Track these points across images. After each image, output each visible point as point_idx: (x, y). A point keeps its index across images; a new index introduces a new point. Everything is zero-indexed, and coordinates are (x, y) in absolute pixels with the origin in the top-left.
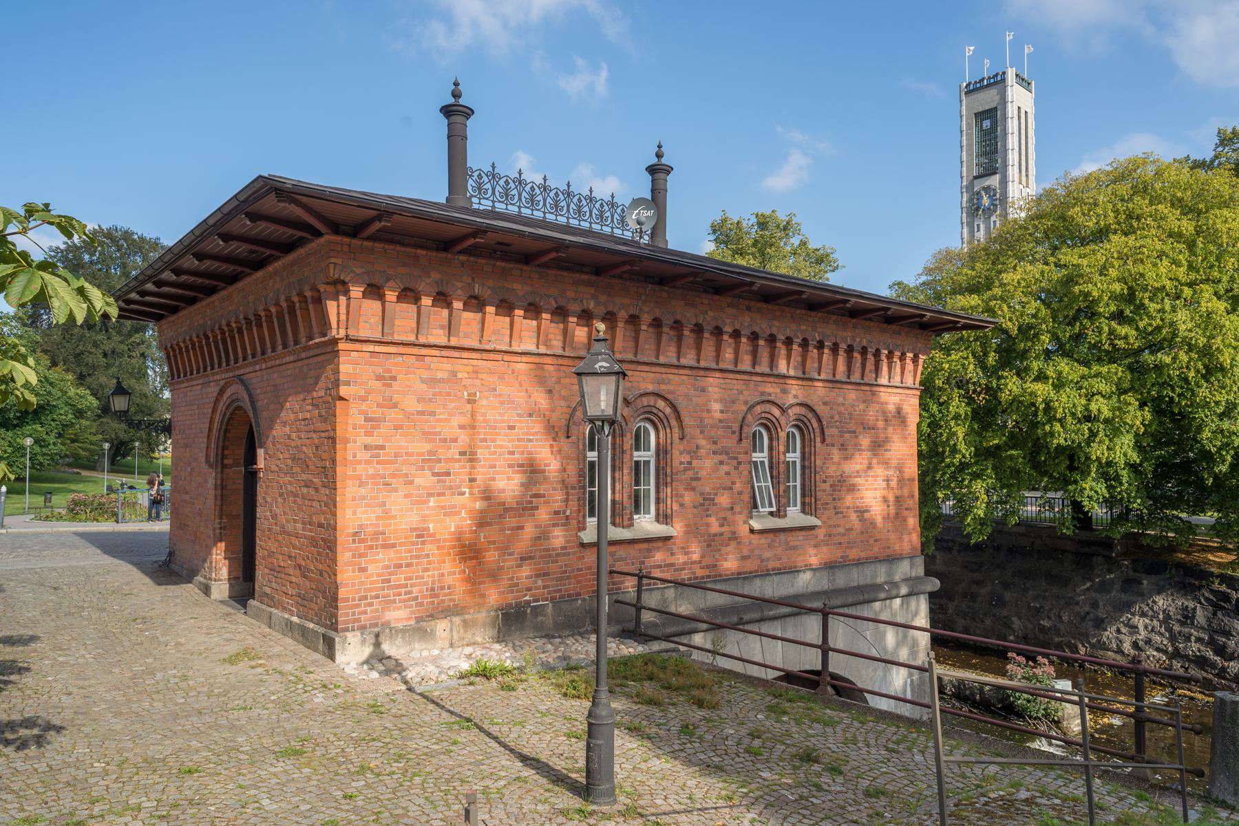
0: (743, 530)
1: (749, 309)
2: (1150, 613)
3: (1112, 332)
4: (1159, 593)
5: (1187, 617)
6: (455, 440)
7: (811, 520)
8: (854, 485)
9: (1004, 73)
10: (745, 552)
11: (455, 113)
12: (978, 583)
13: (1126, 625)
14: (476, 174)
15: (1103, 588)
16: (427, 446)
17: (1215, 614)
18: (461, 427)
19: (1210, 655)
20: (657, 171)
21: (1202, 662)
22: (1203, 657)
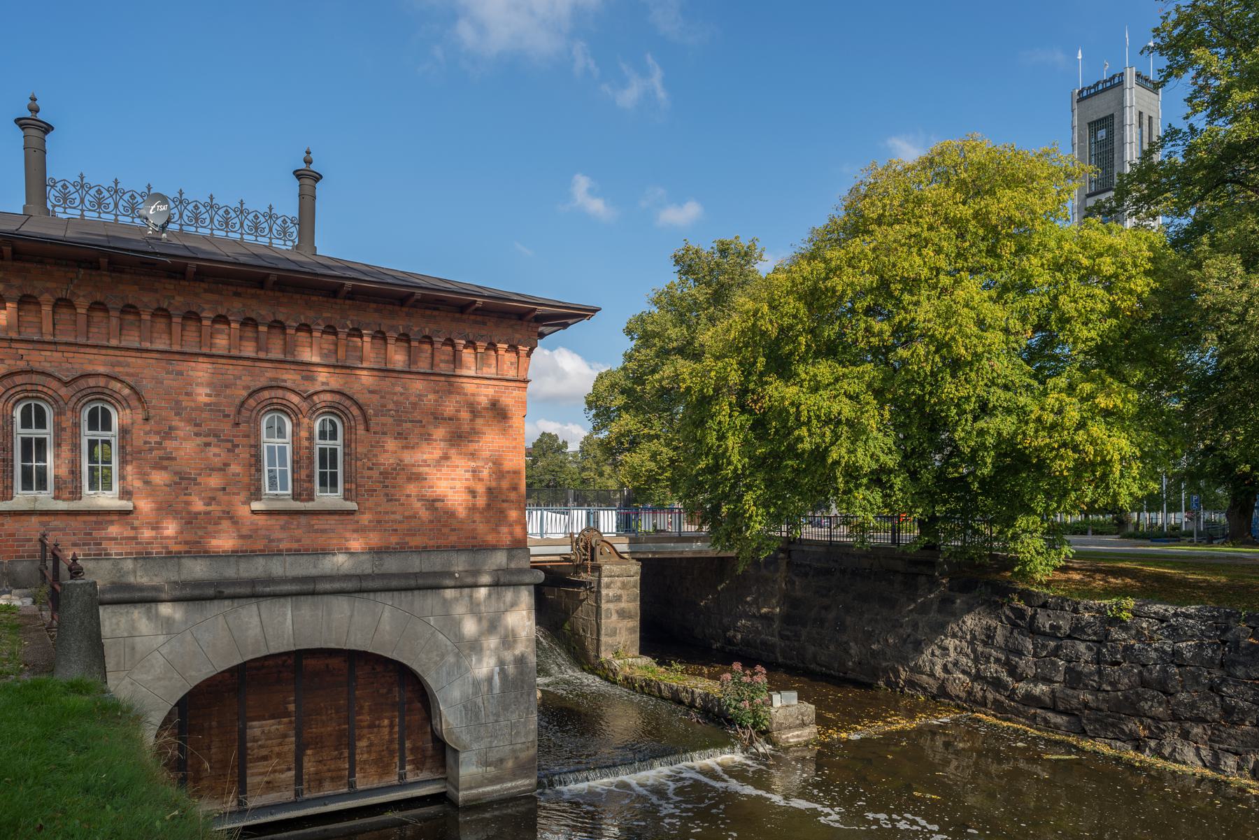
0: (243, 511)
1: (237, 294)
2: (960, 634)
3: (867, 330)
4: (968, 612)
5: (989, 635)
7: (352, 506)
8: (420, 474)
9: (1122, 74)
10: (245, 532)
11: (35, 128)
12: (826, 608)
13: (940, 647)
14: (59, 185)
15: (923, 609)
17: (1011, 633)
19: (1004, 676)
20: (307, 177)
21: (997, 684)
22: (998, 678)
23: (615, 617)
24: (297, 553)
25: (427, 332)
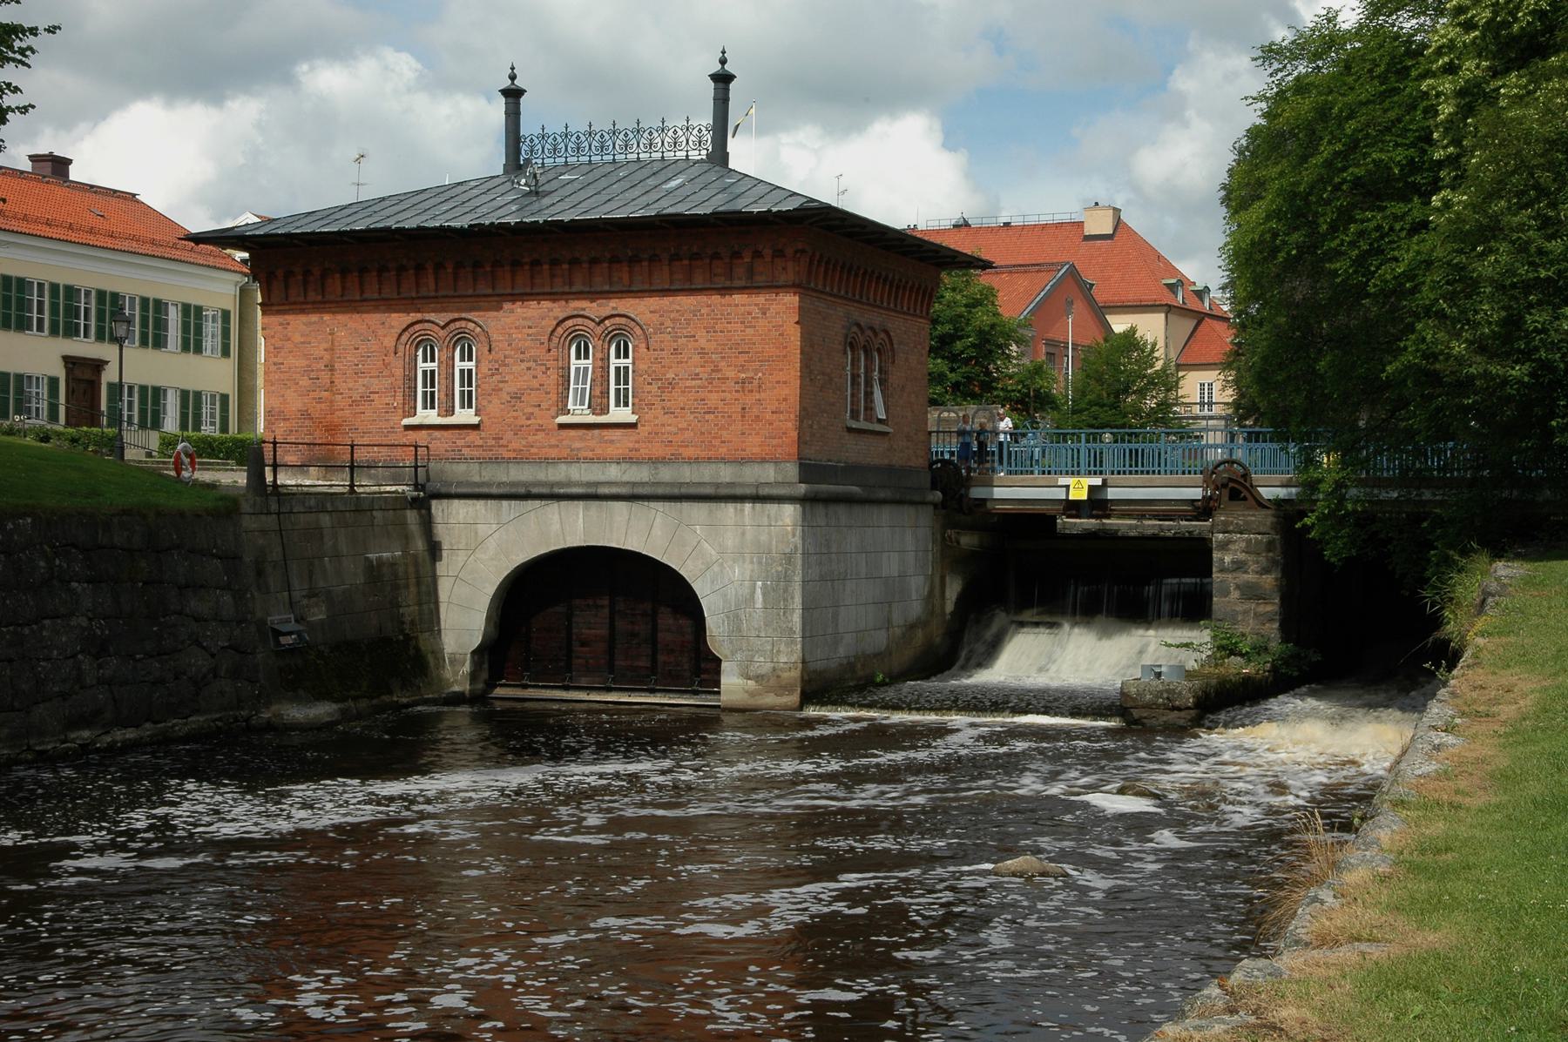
16: (304, 362)
23: (1235, 594)
24: (591, 460)
25: (695, 249)
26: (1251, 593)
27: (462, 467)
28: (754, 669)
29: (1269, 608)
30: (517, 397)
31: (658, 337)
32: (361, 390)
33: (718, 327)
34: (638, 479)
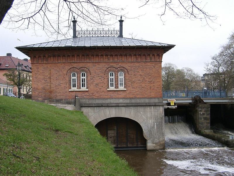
6: (47, 76)
7: (126, 89)
16: (43, 77)
18: (48, 74)
23: (203, 119)
25: (139, 53)
26: (205, 119)
27: (84, 100)
28: (155, 141)
29: (209, 121)
30: (97, 84)
31: (131, 72)
32: (58, 83)
33: (144, 70)
34: (127, 102)
